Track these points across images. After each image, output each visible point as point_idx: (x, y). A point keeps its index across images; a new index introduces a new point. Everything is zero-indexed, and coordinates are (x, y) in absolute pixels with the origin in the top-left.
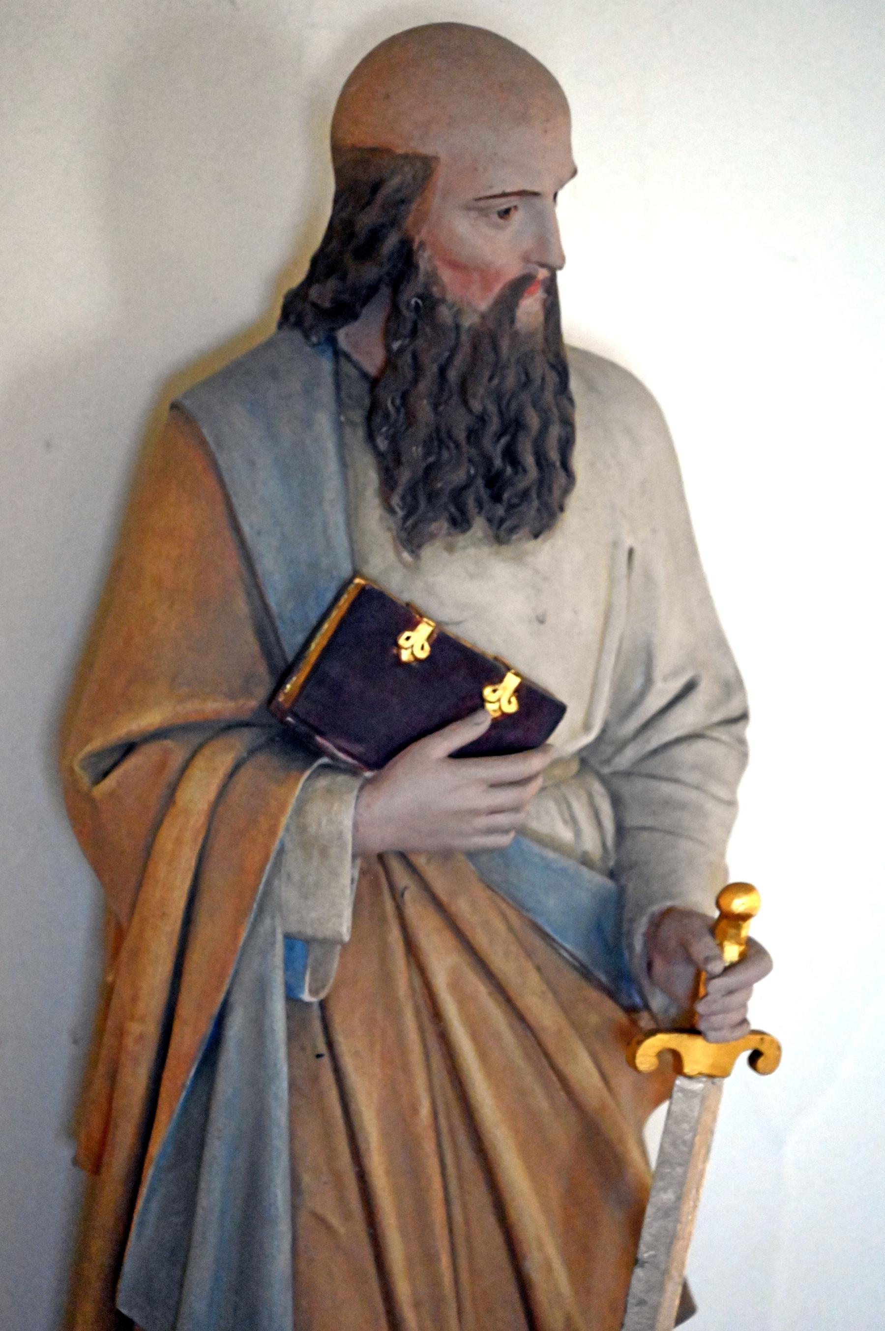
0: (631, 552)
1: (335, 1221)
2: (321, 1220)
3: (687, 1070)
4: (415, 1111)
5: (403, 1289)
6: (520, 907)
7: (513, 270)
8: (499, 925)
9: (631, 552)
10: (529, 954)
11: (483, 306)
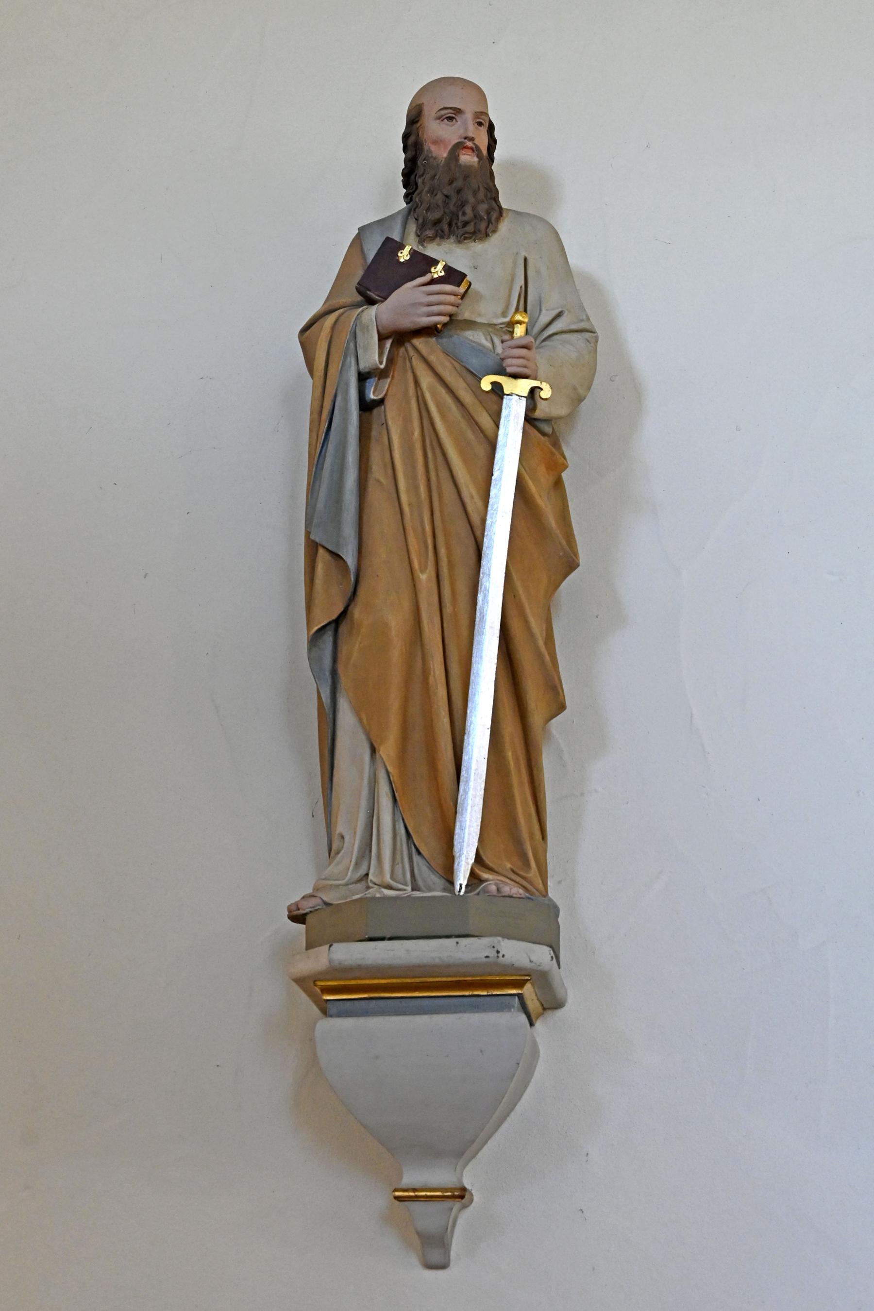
0: (526, 260)
1: (382, 480)
2: (378, 481)
3: (506, 392)
4: (413, 434)
5: (404, 498)
6: (458, 360)
7: (455, 140)
8: (447, 364)
9: (526, 260)
10: (461, 375)
11: (445, 155)
